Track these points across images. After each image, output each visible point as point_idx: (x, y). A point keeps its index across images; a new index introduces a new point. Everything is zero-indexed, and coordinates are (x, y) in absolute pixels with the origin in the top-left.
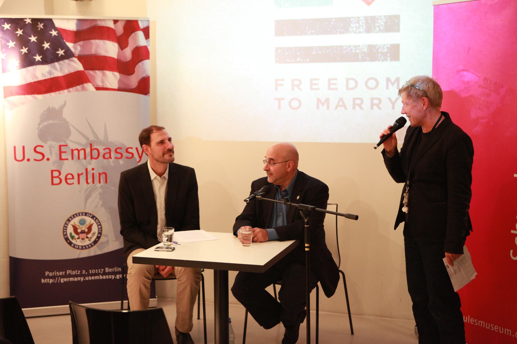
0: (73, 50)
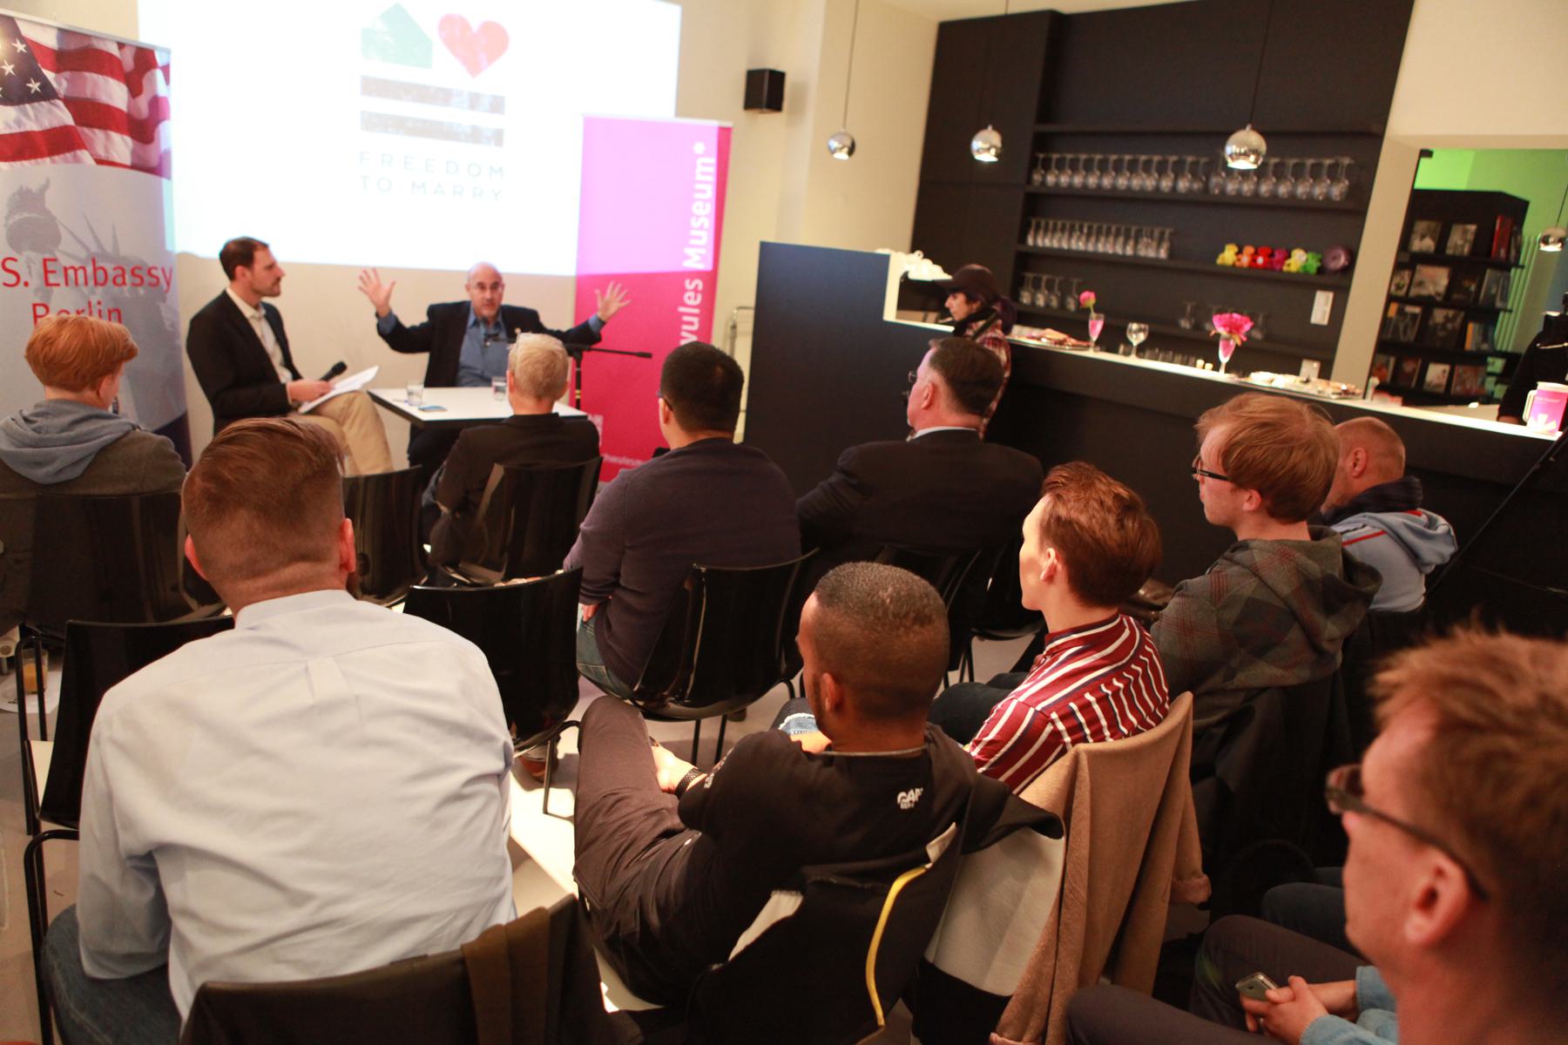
0: (54, 84)
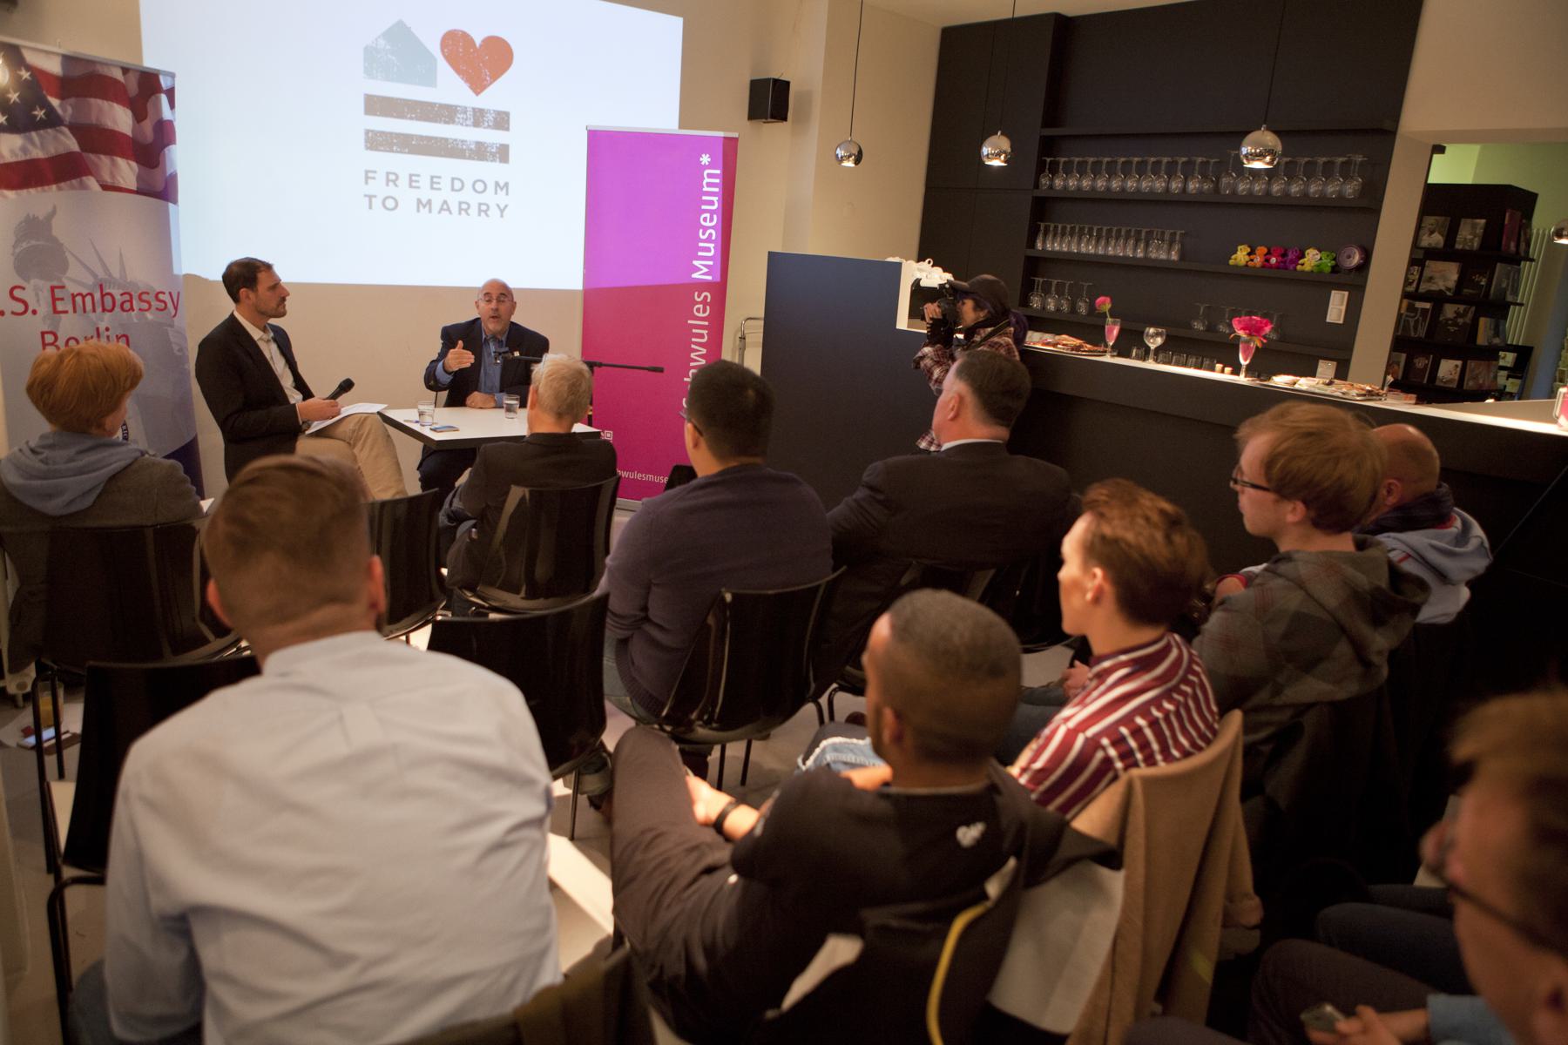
0: (60, 111)
